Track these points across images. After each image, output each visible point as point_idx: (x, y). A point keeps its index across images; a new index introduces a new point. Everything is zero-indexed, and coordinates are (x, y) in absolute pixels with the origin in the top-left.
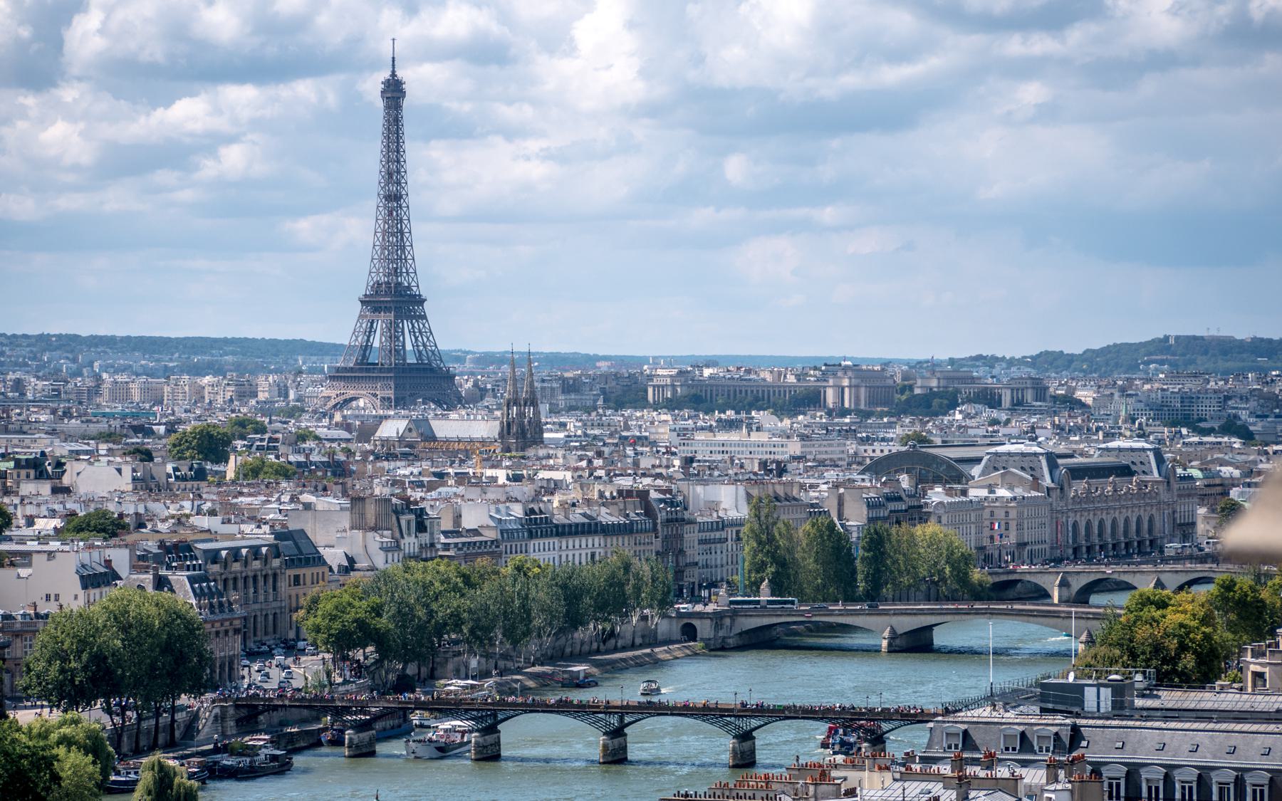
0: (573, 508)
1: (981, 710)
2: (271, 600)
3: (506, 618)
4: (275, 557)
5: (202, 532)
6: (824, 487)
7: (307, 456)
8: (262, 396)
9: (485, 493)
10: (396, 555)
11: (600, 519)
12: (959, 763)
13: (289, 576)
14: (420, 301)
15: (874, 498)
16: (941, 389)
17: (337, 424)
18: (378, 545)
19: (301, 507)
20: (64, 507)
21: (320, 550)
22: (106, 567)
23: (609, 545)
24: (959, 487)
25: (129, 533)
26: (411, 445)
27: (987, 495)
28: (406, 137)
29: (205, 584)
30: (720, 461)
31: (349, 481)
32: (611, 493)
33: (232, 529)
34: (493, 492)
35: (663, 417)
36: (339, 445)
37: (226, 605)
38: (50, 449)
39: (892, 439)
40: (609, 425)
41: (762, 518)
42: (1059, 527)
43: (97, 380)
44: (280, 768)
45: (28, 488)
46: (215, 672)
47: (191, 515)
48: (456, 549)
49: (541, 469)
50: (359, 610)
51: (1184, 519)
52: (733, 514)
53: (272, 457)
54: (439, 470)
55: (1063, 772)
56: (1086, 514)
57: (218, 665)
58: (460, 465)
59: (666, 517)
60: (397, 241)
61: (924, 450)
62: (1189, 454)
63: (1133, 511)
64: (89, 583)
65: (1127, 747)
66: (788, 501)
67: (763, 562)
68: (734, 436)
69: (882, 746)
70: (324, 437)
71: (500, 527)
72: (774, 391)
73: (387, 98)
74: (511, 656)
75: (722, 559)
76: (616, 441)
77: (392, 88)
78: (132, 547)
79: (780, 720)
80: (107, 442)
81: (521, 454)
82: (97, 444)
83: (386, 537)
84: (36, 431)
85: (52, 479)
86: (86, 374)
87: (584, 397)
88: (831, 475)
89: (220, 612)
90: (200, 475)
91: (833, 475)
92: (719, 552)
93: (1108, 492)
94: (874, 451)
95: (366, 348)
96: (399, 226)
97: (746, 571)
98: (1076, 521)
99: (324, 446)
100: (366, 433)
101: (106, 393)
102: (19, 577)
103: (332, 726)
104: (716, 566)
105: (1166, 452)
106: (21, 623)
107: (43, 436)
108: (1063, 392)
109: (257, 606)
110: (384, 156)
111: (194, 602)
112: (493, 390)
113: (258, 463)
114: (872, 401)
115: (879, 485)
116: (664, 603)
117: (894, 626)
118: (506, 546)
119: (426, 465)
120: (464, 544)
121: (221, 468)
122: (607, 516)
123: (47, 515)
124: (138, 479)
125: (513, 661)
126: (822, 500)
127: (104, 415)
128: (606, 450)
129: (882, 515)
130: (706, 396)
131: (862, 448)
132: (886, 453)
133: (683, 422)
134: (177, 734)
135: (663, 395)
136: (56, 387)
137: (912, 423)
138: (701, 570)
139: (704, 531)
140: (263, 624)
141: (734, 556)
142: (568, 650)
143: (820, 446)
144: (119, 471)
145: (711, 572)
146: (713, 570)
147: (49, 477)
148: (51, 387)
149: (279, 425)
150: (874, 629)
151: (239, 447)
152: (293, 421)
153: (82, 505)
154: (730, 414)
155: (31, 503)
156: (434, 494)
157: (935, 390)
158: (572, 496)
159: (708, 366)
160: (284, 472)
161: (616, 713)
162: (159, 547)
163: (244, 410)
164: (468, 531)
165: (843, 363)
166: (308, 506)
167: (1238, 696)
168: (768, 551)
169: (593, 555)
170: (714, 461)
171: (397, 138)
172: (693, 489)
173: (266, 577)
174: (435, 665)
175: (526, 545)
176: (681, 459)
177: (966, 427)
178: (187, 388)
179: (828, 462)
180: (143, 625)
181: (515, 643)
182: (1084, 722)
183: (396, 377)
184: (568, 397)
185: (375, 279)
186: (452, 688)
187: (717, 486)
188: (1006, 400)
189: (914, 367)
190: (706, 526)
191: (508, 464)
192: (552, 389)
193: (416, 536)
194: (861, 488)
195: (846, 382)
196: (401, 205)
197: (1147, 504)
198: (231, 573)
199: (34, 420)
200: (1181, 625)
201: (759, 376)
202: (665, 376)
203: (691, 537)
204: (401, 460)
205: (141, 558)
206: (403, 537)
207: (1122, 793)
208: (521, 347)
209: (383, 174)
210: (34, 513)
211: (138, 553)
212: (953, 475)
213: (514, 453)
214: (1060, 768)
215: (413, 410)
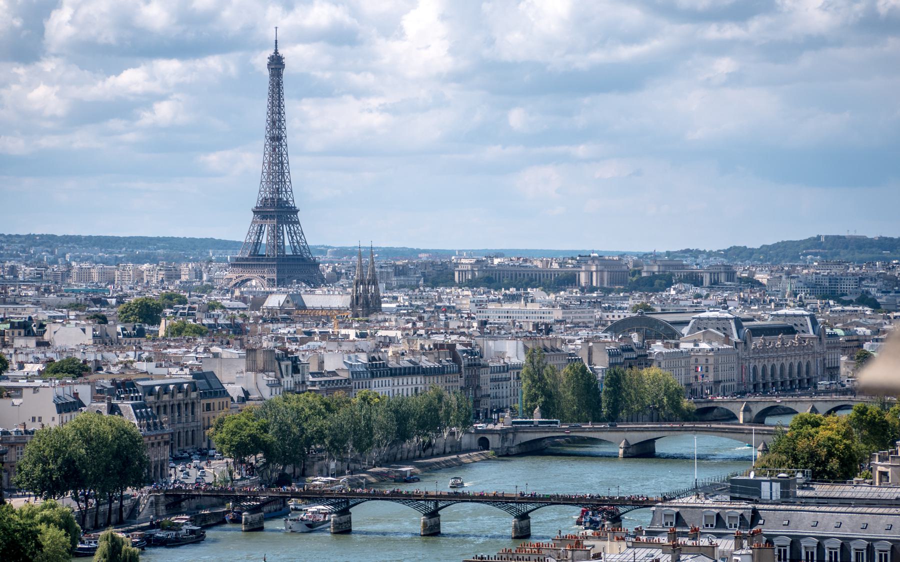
0: (403, 357)
1: (689, 498)
2: (191, 421)
3: (355, 433)
4: (193, 391)
5: (141, 373)
6: (579, 342)
7: (216, 320)
8: (184, 278)
9: (341, 346)
10: (278, 389)
11: (421, 364)
12: (673, 535)
13: (203, 404)
14: (295, 211)
15: (614, 349)
16: (661, 273)
17: (236, 298)
18: (266, 383)
19: (211, 356)
20: (45, 356)
21: (225, 386)
22: (75, 398)
23: (427, 383)
24: (673, 341)
25: (91, 374)
26: (288, 313)
27: (693, 347)
28: (285, 96)
29: (144, 410)
30: (505, 324)
31: (245, 337)
32: (429, 346)
33: (163, 371)
34: (346, 345)
35: (466, 293)
36: (238, 312)
37: (159, 425)
38: (35, 315)
39: (626, 308)
40: (427, 298)
41: (535, 364)
42: (744, 370)
43: (68, 267)
44: (197, 539)
45: (19, 342)
46: (151, 471)
47: (134, 361)
48: (320, 385)
49: (379, 329)
50: (252, 428)
51: (832, 364)
52: (515, 361)
53: (191, 320)
54: (308, 330)
55: (746, 542)
56: (762, 360)
57: (153, 467)
58: (323, 326)
59: (467, 363)
60: (279, 169)
61: (649, 316)
62: (835, 318)
63: (795, 359)
64: (62, 409)
65: (791, 524)
66: (553, 351)
67: (535, 394)
68: (515, 306)
69: (619, 523)
70: (227, 307)
71: (351, 370)
72: (544, 275)
73: (272, 69)
74: (359, 461)
75: (507, 392)
76: (432, 309)
77: (275, 62)
78: (92, 384)
79: (548, 505)
80: (75, 310)
81: (366, 318)
82: (68, 311)
83: (271, 377)
84: (25, 303)
85: (36, 336)
87: (410, 279)
88: (583, 333)
89: (155, 429)
90: (141, 333)
91: (585, 333)
92: (505, 387)
93: (778, 345)
94: (613, 316)
95: (257, 244)
96: (280, 158)
97: (524, 401)
98: (755, 366)
99: (227, 313)
100: (257, 304)
101: (74, 276)
102: (13, 405)
103: (233, 509)
104: (503, 397)
105: (819, 317)
106: (15, 437)
107: (30, 306)
108: (746, 275)
109: (180, 425)
110: (270, 110)
111: (136, 422)
112: (346, 274)
113: (181, 325)
114: (612, 281)
115: (617, 341)
116: (466, 423)
117: (628, 440)
118: (355, 383)
119: (299, 326)
120: (326, 382)
121: (155, 328)
122: (426, 362)
123: (33, 361)
124: (97, 336)
125: (360, 464)
126: (577, 350)
127: (73, 291)
128: (426, 316)
129: (619, 361)
130: (496, 278)
131: (605, 314)
132: (622, 318)
133: (479, 296)
134: (124, 515)
135: (465, 277)
136: (39, 272)
137: (640, 297)
138: (492, 400)
139: (494, 373)
140: (185, 438)
141: (516, 390)
142: (399, 456)
143: (576, 313)
144: (84, 330)
145: (499, 402)
146: (501, 400)
147: (34, 335)
148: (36, 272)
149: (196, 298)
150: (613, 442)
151: (168, 313)
152: (206, 296)
153: (58, 354)
154: (513, 290)
155: (22, 353)
156: (305, 347)
157: (657, 273)
158: (402, 348)
159: (497, 257)
160: (199, 331)
161: (433, 500)
162: (112, 384)
163: (171, 288)
164: (329, 372)
165: (592, 255)
166: (216, 355)
167: (869, 488)
168: (539, 387)
169: (416, 389)
170: (502, 324)
171: (279, 97)
172: (487, 343)
173: (186, 405)
174: (305, 467)
175: (369, 382)
176: (478, 322)
177: (678, 300)
178: (131, 272)
179: (581, 324)
180: (100, 439)
181: (362, 451)
182: (761, 506)
183: (278, 265)
184: (399, 279)
185: (263, 196)
186: (317, 483)
187: (504, 341)
188: (707, 281)
189: (641, 258)
190: (496, 369)
191: (356, 325)
192: (388, 273)
193: (292, 376)
194: (605, 342)
195: (594, 268)
196: (281, 144)
197: (805, 354)
198: (162, 402)
199: (24, 295)
200: (829, 439)
201: (533, 264)
202: (467, 264)
203: (485, 377)
204: (281, 323)
205: (99, 391)
206: (283, 377)
207: (788, 557)
208: (366, 244)
209: (269, 122)
210: (24, 360)
211: (97, 388)
212: (669, 333)
213: (361, 318)
214: (744, 539)
215: (290, 288)
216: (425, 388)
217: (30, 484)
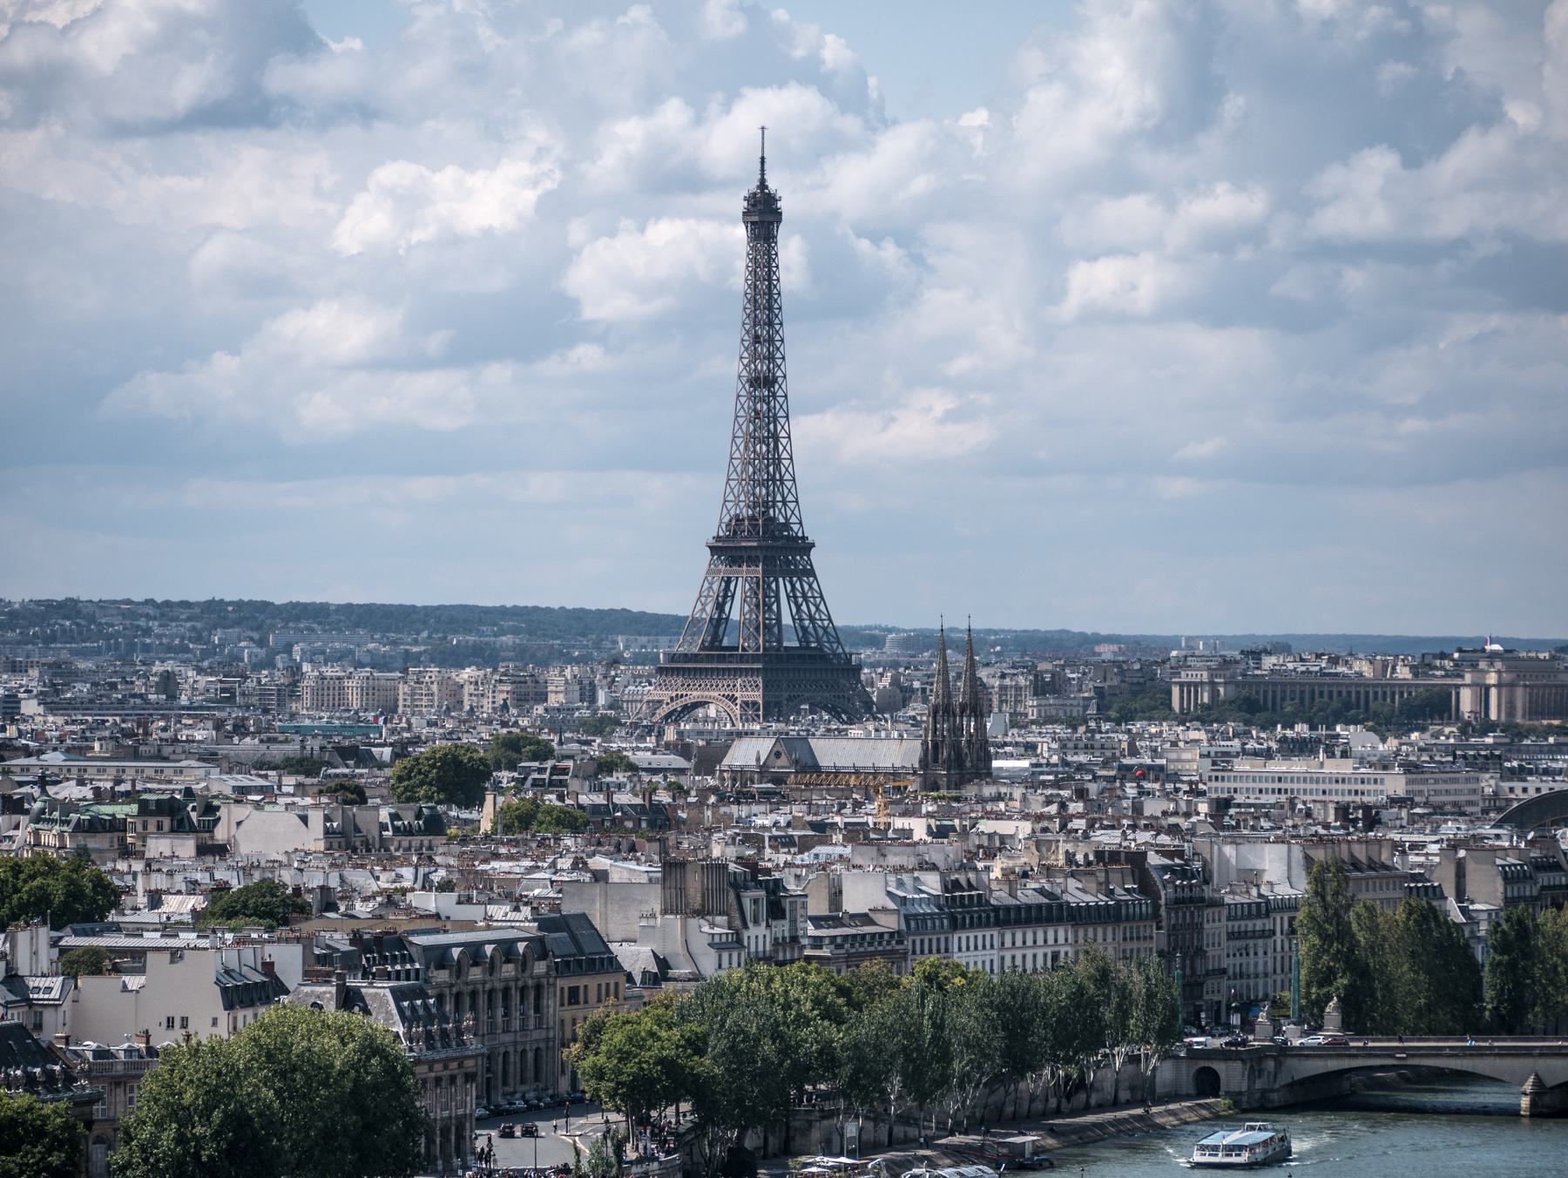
0: (1024, 881)
2: (532, 1027)
3: (908, 1059)
4: (540, 959)
5: (421, 917)
6: (1434, 848)
7: (609, 797)
8: (555, 700)
11: (1066, 897)
13: (562, 989)
14: (805, 547)
15: (1515, 865)
17: (668, 746)
19: (587, 877)
20: (212, 877)
21: (614, 947)
22: (265, 975)
23: (1081, 941)
26: (779, 779)
29: (419, 1002)
30: (1273, 806)
31: (672, 836)
32: (1086, 856)
33: (473, 912)
34: (896, 855)
35: (1193, 735)
37: (453, 1035)
38: (203, 784)
40: (1103, 747)
41: (1329, 898)
43: (294, 674)
45: (158, 846)
46: (434, 1142)
47: (413, 890)
49: (982, 818)
50: (666, 1044)
52: (1284, 891)
53: (553, 797)
54: (819, 818)
58: (854, 811)
60: (768, 451)
64: (235, 999)
66: (1374, 869)
67: (1329, 968)
68: (1298, 766)
70: (645, 765)
71: (903, 912)
72: (1376, 693)
73: (752, 223)
74: (915, 1119)
75: (1266, 963)
76: (1112, 773)
77: (760, 207)
78: (307, 942)
80: (298, 773)
81: (954, 793)
82: (280, 776)
83: (720, 927)
84: (184, 756)
85: (197, 832)
86: (280, 665)
87: (1069, 702)
88: (1450, 828)
89: (443, 1047)
90: (435, 825)
91: (1451, 829)
92: (1261, 953)
95: (719, 623)
96: (772, 426)
97: (1303, 983)
99: (640, 780)
100: (708, 759)
102: (125, 988)
104: (1257, 976)
106: (125, 1063)
107: (193, 763)
109: (508, 1038)
110: (748, 316)
111: (400, 1029)
112: (924, 690)
113: (529, 806)
114: (1535, 711)
115: (1522, 845)
116: (1167, 1034)
117: (1540, 1073)
118: (914, 942)
119: (798, 810)
120: (845, 937)
121: (474, 815)
122: (1077, 893)
123: (183, 888)
124: (334, 833)
125: (918, 1126)
126: (1431, 868)
127: (298, 730)
128: (1093, 788)
129: (1528, 893)
130: (1265, 698)
131: (1506, 785)
133: (1222, 743)
135: (1196, 698)
136: (227, 685)
138: (1231, 982)
139: (1236, 919)
140: (518, 1065)
141: (1287, 960)
142: (1009, 1109)
143: (1437, 782)
144: (304, 819)
145: (1248, 987)
146: (1252, 982)
147: (193, 829)
148: (219, 686)
149: (575, 746)
151: (505, 781)
152: (599, 740)
153: (241, 873)
155: (159, 870)
156: (807, 858)
158: (1023, 860)
159: (1270, 653)
160: (571, 821)
162: (352, 943)
163: (524, 722)
164: (853, 916)
165: (1488, 648)
166: (600, 876)
168: (1338, 951)
169: (1055, 956)
170: (1264, 806)
171: (769, 287)
172: (1220, 849)
173: (523, 990)
174: (792, 1133)
175: (947, 939)
176: (1211, 802)
178: (435, 688)
179: (1448, 808)
180: (319, 1071)
181: (922, 1096)
184: (1043, 702)
185: (732, 513)
186: (814, 1169)
187: (1258, 846)
191: (930, 809)
192: (1018, 688)
193: (768, 926)
194: (1494, 849)
195: (1492, 679)
198: (467, 984)
199: (184, 738)
203: (1215, 927)
204: (759, 803)
205: (322, 960)
206: (746, 926)
208: (956, 621)
211: (317, 951)
213: (944, 792)
215: (795, 723)
216: (1077, 953)
217: (149, 1171)
